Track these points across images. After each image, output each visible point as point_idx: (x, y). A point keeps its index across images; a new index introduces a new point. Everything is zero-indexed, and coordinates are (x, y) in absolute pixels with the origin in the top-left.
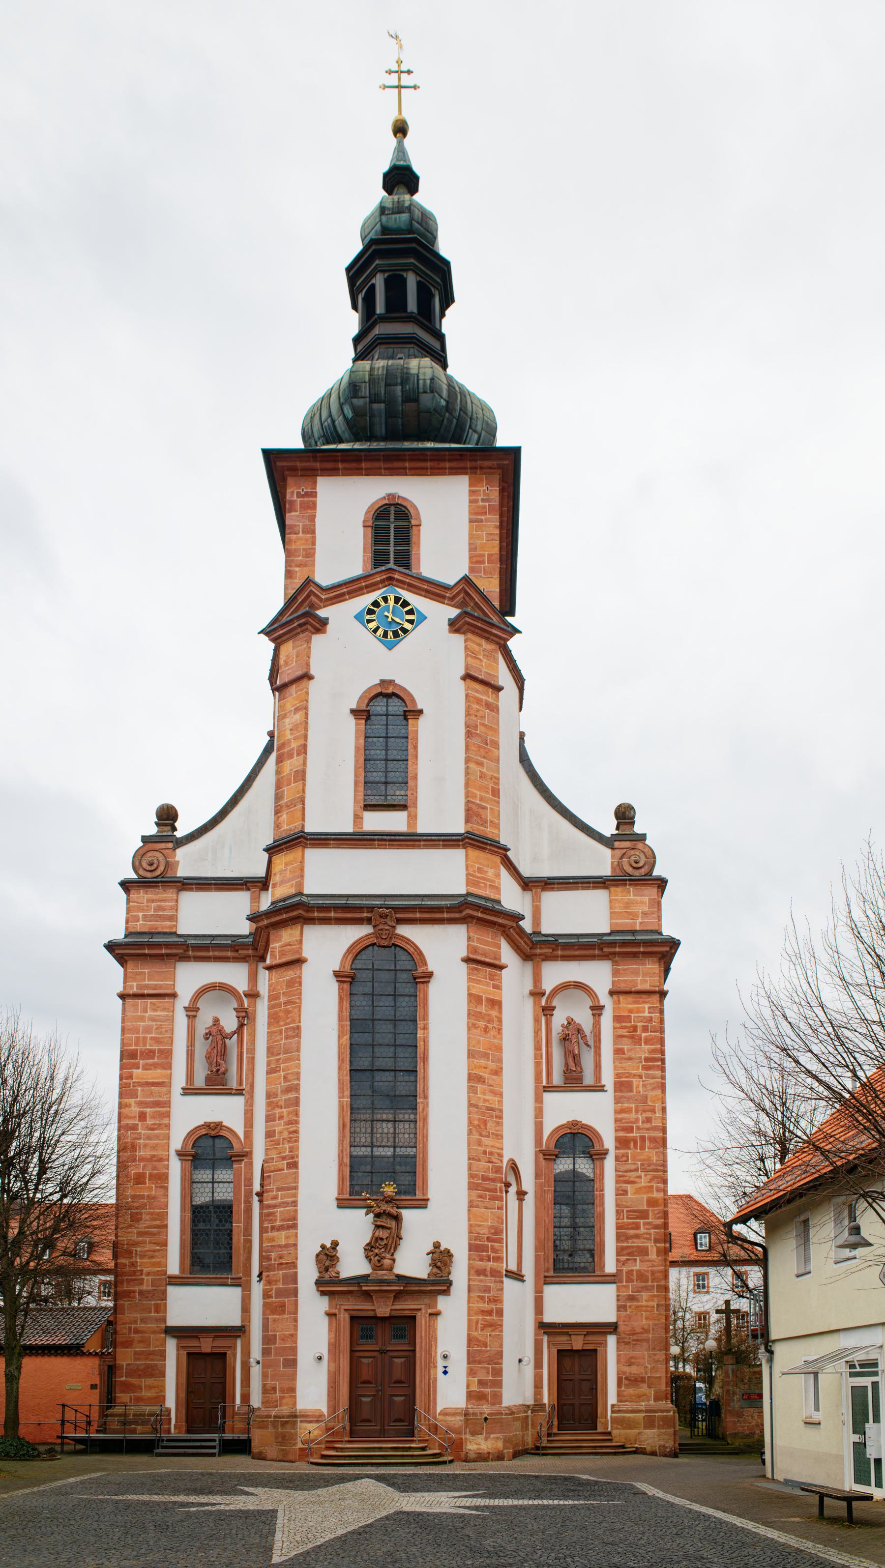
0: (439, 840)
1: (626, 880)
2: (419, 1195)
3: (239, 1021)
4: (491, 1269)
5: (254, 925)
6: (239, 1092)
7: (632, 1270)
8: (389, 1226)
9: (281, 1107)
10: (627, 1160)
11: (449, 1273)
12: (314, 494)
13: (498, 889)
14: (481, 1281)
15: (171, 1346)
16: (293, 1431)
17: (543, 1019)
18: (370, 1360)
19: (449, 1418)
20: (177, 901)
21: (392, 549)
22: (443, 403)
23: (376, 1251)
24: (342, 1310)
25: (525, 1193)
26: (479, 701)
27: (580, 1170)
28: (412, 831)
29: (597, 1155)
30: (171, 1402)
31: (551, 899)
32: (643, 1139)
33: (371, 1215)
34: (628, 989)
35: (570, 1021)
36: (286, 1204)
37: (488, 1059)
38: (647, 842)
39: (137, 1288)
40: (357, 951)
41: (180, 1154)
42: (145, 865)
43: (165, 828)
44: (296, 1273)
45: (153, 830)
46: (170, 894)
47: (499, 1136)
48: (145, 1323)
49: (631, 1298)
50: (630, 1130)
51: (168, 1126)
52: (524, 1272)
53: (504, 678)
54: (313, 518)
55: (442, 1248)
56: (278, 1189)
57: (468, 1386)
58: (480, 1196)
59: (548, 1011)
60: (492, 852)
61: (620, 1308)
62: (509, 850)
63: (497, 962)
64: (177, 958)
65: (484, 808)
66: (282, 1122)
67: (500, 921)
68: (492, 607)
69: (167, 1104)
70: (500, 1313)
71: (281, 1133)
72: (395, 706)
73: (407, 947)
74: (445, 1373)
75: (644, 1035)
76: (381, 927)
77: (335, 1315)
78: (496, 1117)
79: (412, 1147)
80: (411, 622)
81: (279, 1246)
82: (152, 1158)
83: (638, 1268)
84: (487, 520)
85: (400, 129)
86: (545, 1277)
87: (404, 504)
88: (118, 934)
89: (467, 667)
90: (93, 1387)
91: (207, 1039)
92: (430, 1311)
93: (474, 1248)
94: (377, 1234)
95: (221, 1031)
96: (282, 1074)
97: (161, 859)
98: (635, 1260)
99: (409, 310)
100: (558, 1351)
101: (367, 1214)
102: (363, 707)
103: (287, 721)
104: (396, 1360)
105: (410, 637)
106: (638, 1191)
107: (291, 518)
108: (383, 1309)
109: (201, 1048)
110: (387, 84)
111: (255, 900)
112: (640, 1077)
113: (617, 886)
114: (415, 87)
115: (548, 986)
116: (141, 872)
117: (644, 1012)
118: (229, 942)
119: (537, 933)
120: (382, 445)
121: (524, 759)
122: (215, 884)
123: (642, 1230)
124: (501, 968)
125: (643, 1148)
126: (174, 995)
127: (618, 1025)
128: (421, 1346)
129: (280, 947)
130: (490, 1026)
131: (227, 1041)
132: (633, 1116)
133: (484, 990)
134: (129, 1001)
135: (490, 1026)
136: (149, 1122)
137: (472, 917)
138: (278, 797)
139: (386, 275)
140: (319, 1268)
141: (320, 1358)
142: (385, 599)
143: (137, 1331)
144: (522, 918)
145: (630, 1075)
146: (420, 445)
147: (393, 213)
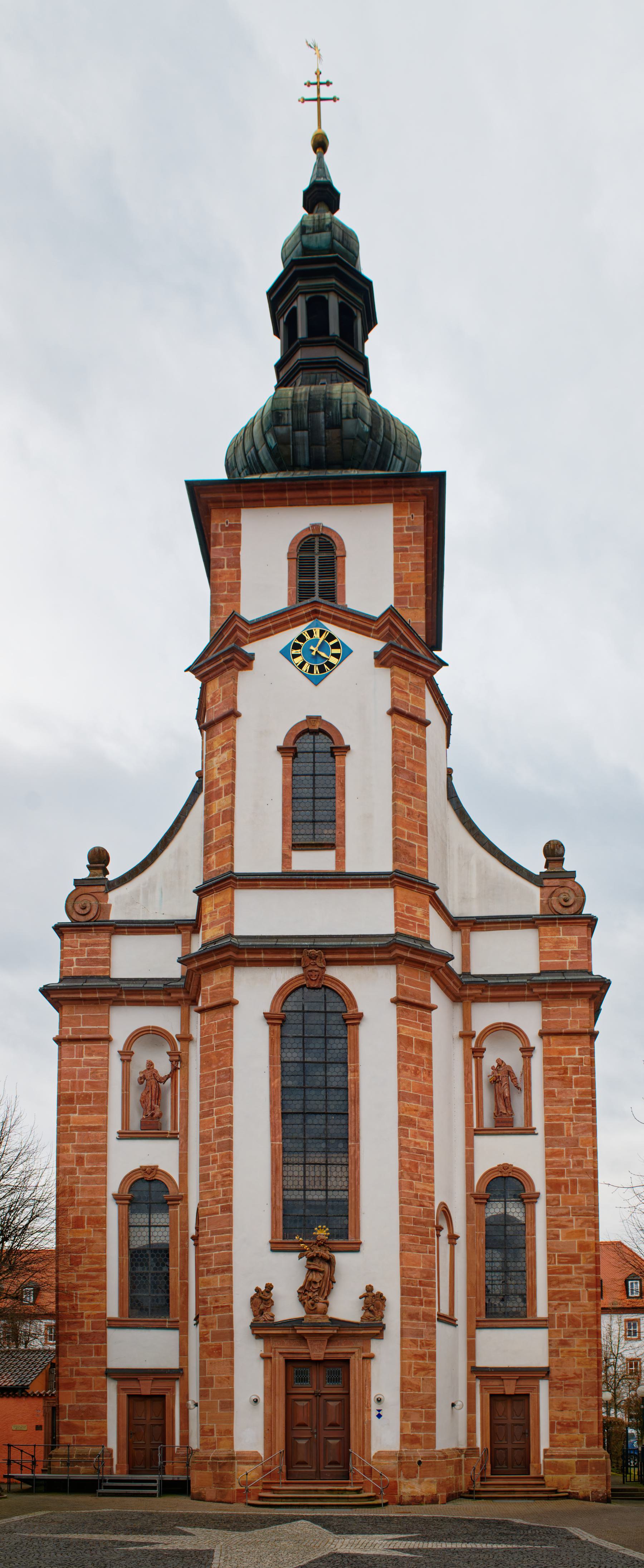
0: (367, 880)
1: (555, 919)
2: (351, 1239)
3: (172, 1065)
4: (424, 1313)
5: (186, 968)
6: (174, 1137)
7: (564, 1315)
8: (322, 1269)
9: (215, 1151)
10: (559, 1204)
11: (382, 1317)
12: (238, 527)
13: (426, 929)
14: (414, 1325)
15: (112, 1388)
16: (231, 1473)
17: (473, 1061)
18: (305, 1403)
19: (383, 1462)
20: (110, 945)
21: (317, 581)
22: (367, 429)
23: (310, 1294)
24: (277, 1354)
25: (457, 1237)
26: (406, 737)
27: (511, 1214)
28: (340, 870)
29: (528, 1199)
30: (112, 1443)
31: (480, 940)
32: (574, 1182)
33: (305, 1259)
34: (558, 1030)
35: (500, 1063)
36: (221, 1248)
37: (418, 1102)
38: (576, 880)
39: (77, 1331)
40: (286, 993)
41: (117, 1198)
42: (78, 909)
43: (96, 871)
44: (231, 1317)
45: (85, 874)
46: (103, 938)
47: (430, 1180)
48: (87, 1365)
49: (563, 1343)
50: (562, 1173)
51: (105, 1171)
52: (456, 1316)
53: (431, 712)
54: (237, 552)
55: (375, 1292)
56: (213, 1233)
57: (402, 1430)
58: (412, 1240)
59: (478, 1053)
60: (421, 891)
61: (552, 1353)
62: (437, 888)
63: (427, 1004)
64: (111, 1002)
65: (414, 846)
66: (215, 1165)
67: (429, 961)
68: (418, 639)
69: (104, 1148)
70: (433, 1357)
71: (214, 1176)
72: (323, 743)
73: (337, 988)
74: (379, 1416)
75: (574, 1077)
76: (311, 968)
77: (270, 1358)
78: (427, 1160)
79: (344, 1190)
80: (337, 656)
81: (215, 1289)
82: (90, 1203)
83: (570, 1312)
84: (412, 549)
85: (320, 144)
86: (477, 1321)
87: (329, 534)
88: (53, 978)
89: (393, 701)
90: (38, 1428)
91: (141, 1083)
92: (363, 1355)
93: (406, 1292)
94: (310, 1278)
95: (155, 1074)
96: (215, 1117)
97: (94, 902)
98: (567, 1305)
99: (331, 333)
100: (491, 1395)
101: (300, 1257)
102: (291, 745)
103: (215, 760)
104: (331, 1403)
105: (336, 672)
106: (569, 1235)
107: (216, 551)
108: (317, 1352)
109: (135, 1096)
110: (306, 97)
111: (186, 943)
112: (571, 1119)
113: (546, 925)
114: (334, 99)
115: (479, 1026)
116: (75, 916)
117: (574, 1054)
118: (162, 986)
119: (466, 974)
120: (306, 474)
121: (452, 796)
122: (147, 927)
123: (574, 1274)
124: (431, 1009)
125: (574, 1192)
126: (109, 1040)
127: (548, 1067)
128: (355, 1390)
129: (212, 989)
130: (421, 1068)
131: (161, 1085)
132: (564, 1159)
133: (413, 1031)
134: (65, 1045)
135: (421, 1068)
136: (87, 1166)
137: (401, 958)
138: (207, 837)
139: (308, 297)
140: (254, 1311)
141: (256, 1401)
142: (311, 633)
143: (78, 1373)
144: (451, 958)
145: (560, 1118)
146: (344, 473)
147: (314, 232)
